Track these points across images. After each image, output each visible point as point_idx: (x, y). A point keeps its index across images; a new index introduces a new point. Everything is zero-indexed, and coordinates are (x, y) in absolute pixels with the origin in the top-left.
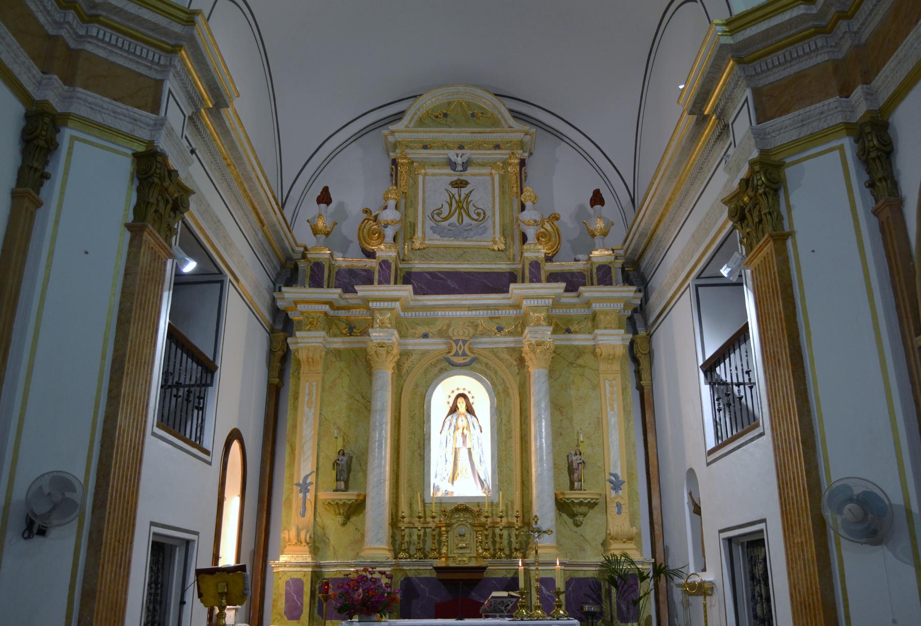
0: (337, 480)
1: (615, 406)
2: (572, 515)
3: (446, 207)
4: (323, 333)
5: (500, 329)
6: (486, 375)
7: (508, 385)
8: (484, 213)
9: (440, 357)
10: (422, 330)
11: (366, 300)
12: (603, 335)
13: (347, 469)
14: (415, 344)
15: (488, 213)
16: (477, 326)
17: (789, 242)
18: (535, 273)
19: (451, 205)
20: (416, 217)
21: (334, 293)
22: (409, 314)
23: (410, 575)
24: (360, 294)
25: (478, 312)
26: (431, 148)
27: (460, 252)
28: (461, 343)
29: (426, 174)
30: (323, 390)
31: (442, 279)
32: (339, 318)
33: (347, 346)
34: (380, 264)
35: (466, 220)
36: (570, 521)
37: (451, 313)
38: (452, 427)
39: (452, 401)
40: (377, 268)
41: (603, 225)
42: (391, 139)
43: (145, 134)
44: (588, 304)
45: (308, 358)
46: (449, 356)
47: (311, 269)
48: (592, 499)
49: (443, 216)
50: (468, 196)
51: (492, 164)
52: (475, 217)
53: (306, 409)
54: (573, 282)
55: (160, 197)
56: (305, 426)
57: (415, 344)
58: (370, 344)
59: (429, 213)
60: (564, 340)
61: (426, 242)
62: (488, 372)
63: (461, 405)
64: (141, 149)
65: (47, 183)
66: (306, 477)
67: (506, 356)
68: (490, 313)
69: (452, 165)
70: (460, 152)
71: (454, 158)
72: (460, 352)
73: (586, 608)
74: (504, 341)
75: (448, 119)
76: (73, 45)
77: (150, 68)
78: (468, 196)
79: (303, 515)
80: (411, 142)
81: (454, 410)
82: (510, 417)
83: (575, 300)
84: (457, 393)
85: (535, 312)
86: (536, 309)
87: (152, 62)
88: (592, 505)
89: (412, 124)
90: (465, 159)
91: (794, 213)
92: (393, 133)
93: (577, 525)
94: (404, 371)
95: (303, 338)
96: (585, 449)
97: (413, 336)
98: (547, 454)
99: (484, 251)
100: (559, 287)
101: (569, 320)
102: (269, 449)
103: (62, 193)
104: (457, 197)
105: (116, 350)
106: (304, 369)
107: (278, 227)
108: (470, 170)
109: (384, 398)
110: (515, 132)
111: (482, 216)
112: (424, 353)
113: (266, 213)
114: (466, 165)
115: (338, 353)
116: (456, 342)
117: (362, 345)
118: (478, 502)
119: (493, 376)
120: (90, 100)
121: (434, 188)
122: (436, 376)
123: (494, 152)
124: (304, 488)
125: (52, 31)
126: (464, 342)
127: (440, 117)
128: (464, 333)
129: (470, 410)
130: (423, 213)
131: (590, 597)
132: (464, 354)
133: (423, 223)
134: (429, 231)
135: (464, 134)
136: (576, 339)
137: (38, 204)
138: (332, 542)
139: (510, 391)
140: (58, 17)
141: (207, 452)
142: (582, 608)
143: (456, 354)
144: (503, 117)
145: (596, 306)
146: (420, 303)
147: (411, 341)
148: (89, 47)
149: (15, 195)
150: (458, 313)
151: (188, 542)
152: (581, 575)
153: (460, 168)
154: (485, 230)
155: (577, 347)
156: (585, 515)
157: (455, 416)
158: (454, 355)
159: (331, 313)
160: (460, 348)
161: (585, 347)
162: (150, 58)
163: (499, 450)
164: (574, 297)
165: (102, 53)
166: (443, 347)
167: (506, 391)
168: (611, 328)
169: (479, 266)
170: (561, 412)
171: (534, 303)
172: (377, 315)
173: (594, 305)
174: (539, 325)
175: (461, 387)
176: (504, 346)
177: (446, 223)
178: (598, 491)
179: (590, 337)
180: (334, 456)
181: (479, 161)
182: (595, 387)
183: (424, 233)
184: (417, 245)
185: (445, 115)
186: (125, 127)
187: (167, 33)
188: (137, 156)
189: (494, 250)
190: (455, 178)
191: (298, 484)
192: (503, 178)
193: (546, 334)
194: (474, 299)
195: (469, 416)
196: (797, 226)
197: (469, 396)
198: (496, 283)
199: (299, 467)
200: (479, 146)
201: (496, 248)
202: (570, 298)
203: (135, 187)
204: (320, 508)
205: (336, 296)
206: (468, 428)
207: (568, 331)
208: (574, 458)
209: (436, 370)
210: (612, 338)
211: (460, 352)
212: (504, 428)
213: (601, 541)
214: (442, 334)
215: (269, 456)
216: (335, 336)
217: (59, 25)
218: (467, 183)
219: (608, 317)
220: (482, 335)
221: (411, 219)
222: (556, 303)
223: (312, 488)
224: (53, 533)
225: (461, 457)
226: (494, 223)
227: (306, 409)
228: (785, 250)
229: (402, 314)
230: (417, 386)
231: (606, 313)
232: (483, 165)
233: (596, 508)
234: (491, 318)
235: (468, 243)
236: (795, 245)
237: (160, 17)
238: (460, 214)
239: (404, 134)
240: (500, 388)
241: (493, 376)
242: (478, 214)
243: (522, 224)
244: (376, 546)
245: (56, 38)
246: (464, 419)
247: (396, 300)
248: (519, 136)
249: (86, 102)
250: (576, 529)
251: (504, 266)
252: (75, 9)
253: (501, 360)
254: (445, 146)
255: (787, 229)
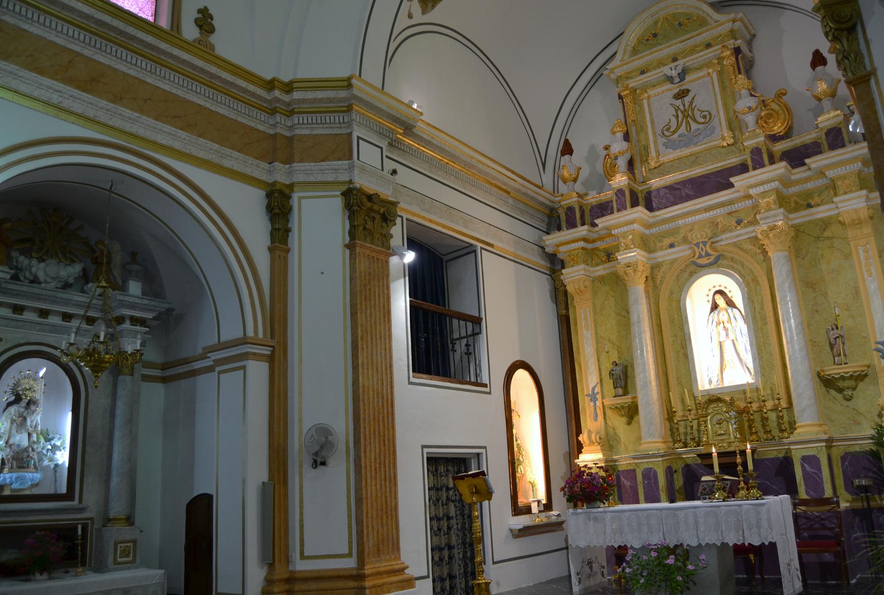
0: (615, 388)
1: (873, 271)
2: (840, 390)
3: (674, 120)
4: (583, 266)
5: (739, 222)
6: (733, 269)
7: (756, 274)
8: (710, 114)
9: (688, 262)
10: (667, 241)
11: (609, 229)
12: (842, 201)
13: (622, 378)
14: (664, 255)
15: (714, 113)
16: (717, 224)
17: (873, 82)
18: (758, 159)
19: (677, 117)
20: (647, 139)
21: (582, 231)
22: (654, 230)
23: (689, 462)
24: (600, 226)
25: (715, 212)
26: (648, 71)
27: (694, 158)
28: (701, 245)
29: (649, 97)
30: (595, 313)
31: (679, 189)
32: (597, 249)
33: (608, 271)
34: (616, 194)
35: (694, 126)
36: (839, 396)
37: (690, 219)
38: (715, 323)
39: (710, 298)
40: (614, 198)
41: (825, 86)
42: (613, 76)
43: (345, 177)
44: (821, 173)
45: (575, 290)
46: (694, 259)
47: (566, 214)
48: (854, 372)
49: (672, 130)
50: (691, 103)
51: (708, 64)
52: (702, 120)
53: (585, 332)
54: (796, 158)
55: (367, 218)
56: (586, 346)
57: (664, 256)
58: (618, 266)
59: (659, 131)
60: (801, 217)
61: (661, 159)
62: (735, 266)
63: (720, 300)
64: (344, 188)
65: (290, 234)
66: (594, 388)
67: (749, 246)
68: (727, 209)
69: (670, 79)
70: (673, 65)
71: (669, 73)
72: (703, 254)
73: (857, 482)
74: (743, 233)
75: (659, 37)
76: (288, 134)
77: (340, 128)
78: (691, 103)
79: (596, 420)
80: (630, 72)
81: (715, 307)
82: (762, 304)
83: (808, 173)
84: (714, 290)
85: (763, 198)
86: (764, 194)
87: (339, 123)
88: (860, 377)
89: (626, 57)
90: (679, 70)
91: (873, 46)
92: (612, 71)
93: (848, 400)
94: (658, 281)
95: (568, 274)
96: (846, 322)
97: (662, 249)
98: (797, 334)
99: (714, 149)
100: (781, 167)
101: (809, 194)
102: (569, 369)
103: (300, 238)
104: (682, 107)
105: (352, 334)
106: (577, 299)
107: (523, 190)
108: (688, 78)
109: (641, 310)
110: (722, 24)
111: (708, 117)
112: (673, 262)
113: (505, 184)
114: (682, 75)
115: (602, 279)
116: (697, 245)
117: (613, 270)
118: (741, 390)
119: (740, 268)
120: (303, 168)
121: (659, 106)
122: (687, 280)
123: (706, 52)
124: (593, 398)
125: (272, 132)
126: (705, 243)
127: (652, 38)
128: (702, 235)
129: (730, 304)
130: (654, 133)
131: (870, 470)
132: (707, 255)
133: (655, 142)
134: (661, 148)
135: (675, 46)
136: (818, 212)
137: (288, 251)
138: (623, 440)
139: (759, 279)
140: (272, 122)
141: (485, 386)
142: (852, 483)
143: (700, 256)
144: (708, 15)
145: (830, 173)
146: (659, 218)
147: (659, 254)
148: (298, 132)
149: (271, 250)
150: (697, 217)
151: (478, 455)
152: (857, 449)
153: (677, 80)
154: (714, 128)
155: (822, 220)
156: (854, 389)
157: (716, 312)
158: (699, 258)
159: (589, 246)
160: (702, 249)
161: (830, 218)
162: (337, 121)
163: (756, 337)
164: (806, 170)
165: (306, 132)
166: (689, 252)
167: (755, 280)
168: (851, 191)
169: (711, 167)
170: (814, 289)
171: (761, 189)
172: (622, 240)
173: (827, 173)
174: (770, 209)
175: (717, 285)
176: (746, 237)
177: (675, 136)
178: (866, 362)
179: (833, 206)
180: (610, 367)
181: (695, 65)
182: (848, 256)
183: (657, 152)
184: (653, 164)
185: (655, 35)
186: (331, 178)
187: (339, 100)
188: (344, 194)
189: (724, 147)
190: (676, 91)
191: (588, 395)
192: (720, 73)
193: (779, 219)
194: (707, 201)
195: (730, 310)
196: (877, 63)
197: (726, 291)
198: (719, 181)
199: (587, 380)
200: (692, 51)
201: (725, 144)
202: (799, 173)
203: (346, 217)
204: (608, 412)
205: (585, 233)
206: (729, 321)
207: (810, 206)
208: (832, 332)
209: (687, 274)
210: (853, 202)
211: (703, 254)
212: (758, 316)
213: (877, 412)
214: (685, 240)
215: (569, 374)
216: (598, 265)
217: (274, 126)
218: (688, 91)
219: (847, 181)
220: (723, 232)
221: (644, 143)
222: (786, 182)
223: (599, 396)
224: (331, 462)
225: (721, 351)
226: (720, 120)
227: (585, 332)
228: (869, 92)
229: (647, 232)
230: (672, 293)
231: (843, 178)
232: (700, 68)
233: (866, 379)
234: (730, 214)
235: (699, 148)
236: (877, 82)
237: (329, 92)
238: (688, 123)
239: (621, 68)
240: (749, 278)
241: (740, 268)
242: (704, 117)
243: (739, 115)
244: (650, 440)
245: (274, 136)
246: (725, 313)
247: (632, 222)
248: (728, 26)
249: (303, 171)
250: (846, 403)
251: (735, 160)
252: (278, 112)
253: (745, 251)
254: (661, 64)
255: (869, 68)
